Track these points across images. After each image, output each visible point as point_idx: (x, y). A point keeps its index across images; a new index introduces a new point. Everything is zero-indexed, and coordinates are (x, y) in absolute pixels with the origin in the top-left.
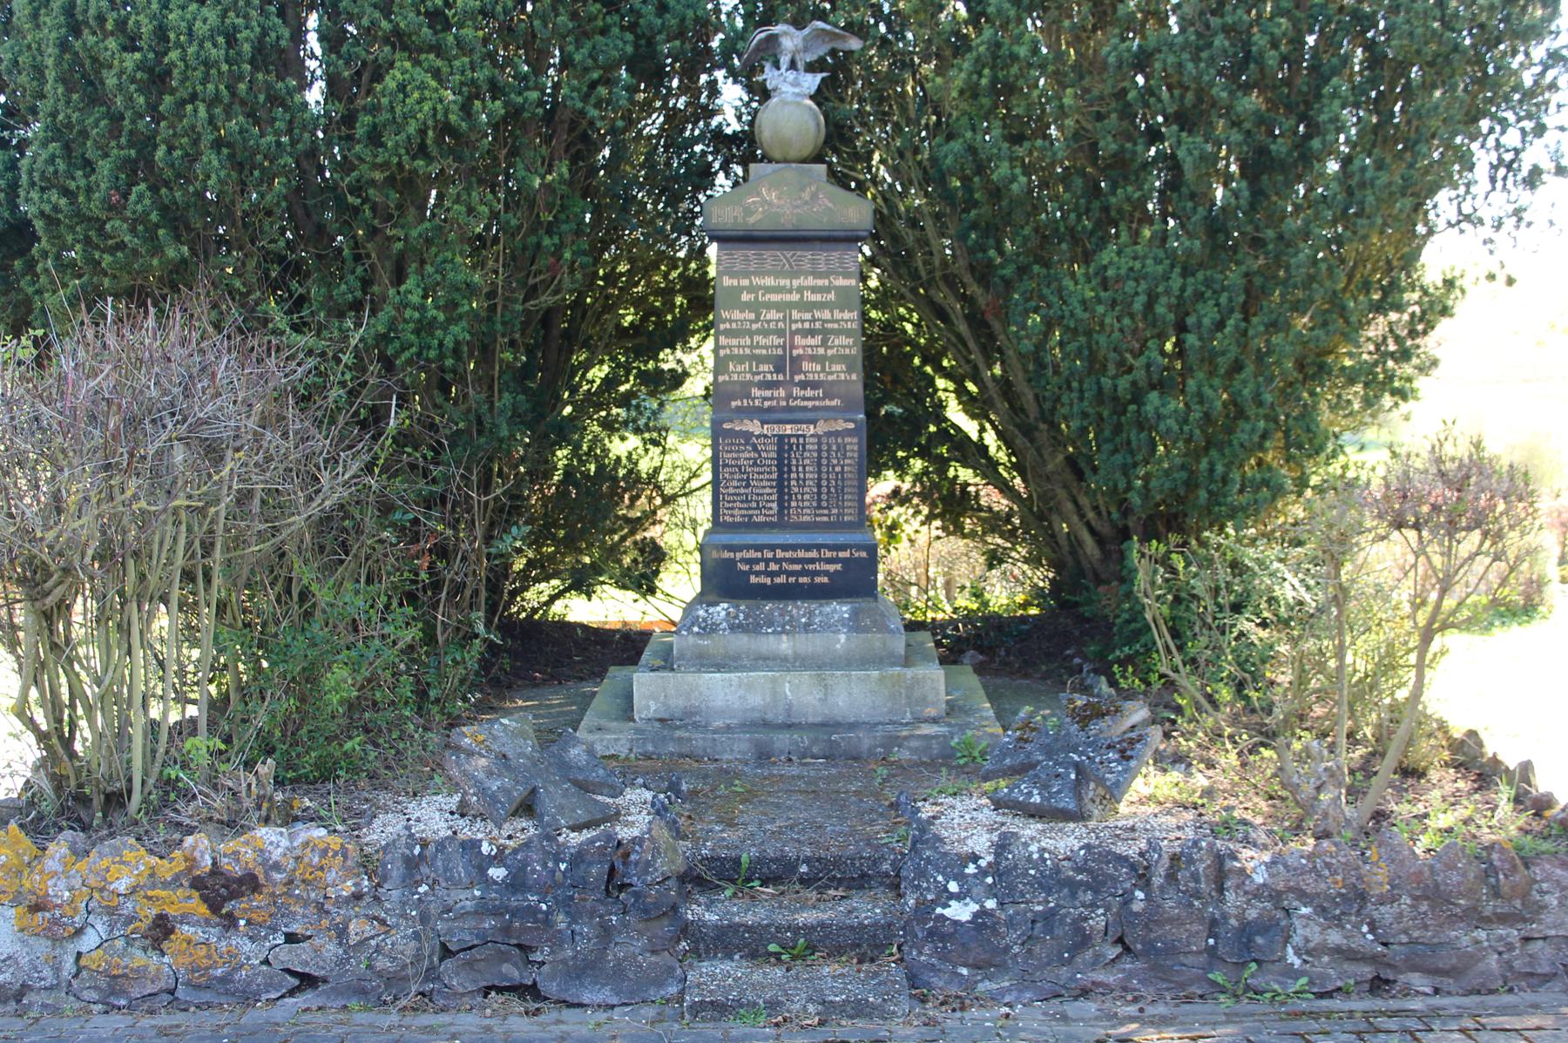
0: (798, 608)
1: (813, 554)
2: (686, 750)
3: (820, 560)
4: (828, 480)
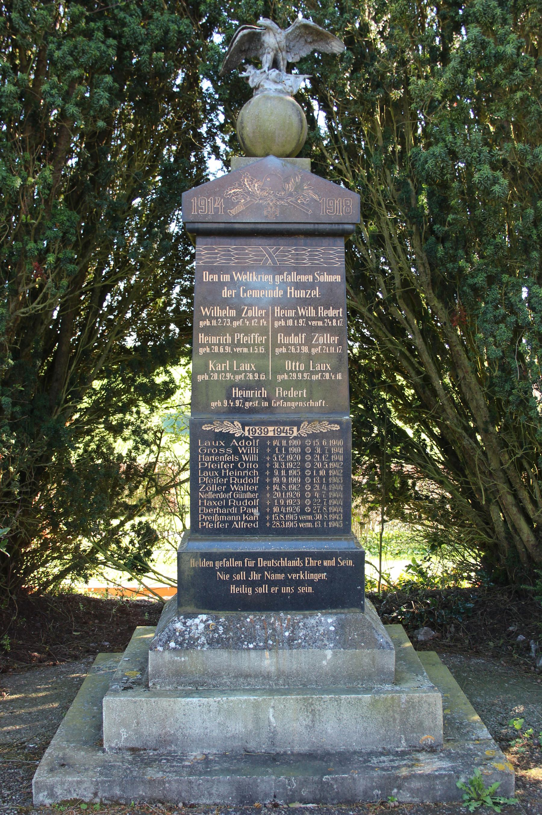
0: (280, 620)
1: (297, 563)
2: (158, 793)
3: (304, 569)
4: (312, 483)
